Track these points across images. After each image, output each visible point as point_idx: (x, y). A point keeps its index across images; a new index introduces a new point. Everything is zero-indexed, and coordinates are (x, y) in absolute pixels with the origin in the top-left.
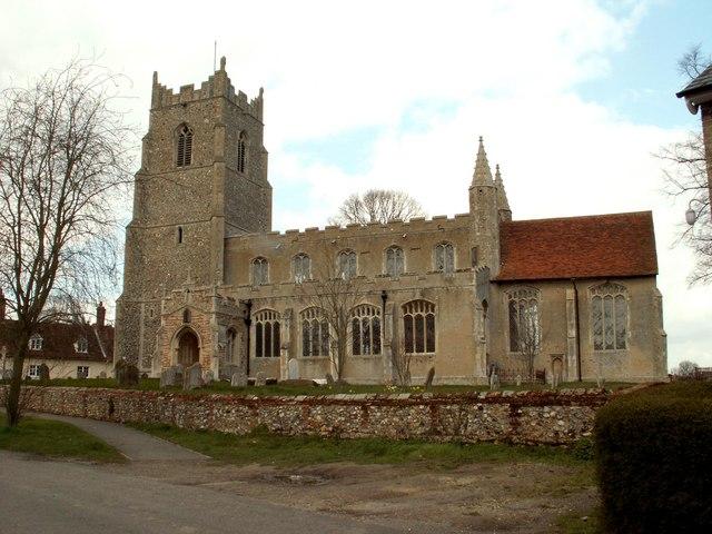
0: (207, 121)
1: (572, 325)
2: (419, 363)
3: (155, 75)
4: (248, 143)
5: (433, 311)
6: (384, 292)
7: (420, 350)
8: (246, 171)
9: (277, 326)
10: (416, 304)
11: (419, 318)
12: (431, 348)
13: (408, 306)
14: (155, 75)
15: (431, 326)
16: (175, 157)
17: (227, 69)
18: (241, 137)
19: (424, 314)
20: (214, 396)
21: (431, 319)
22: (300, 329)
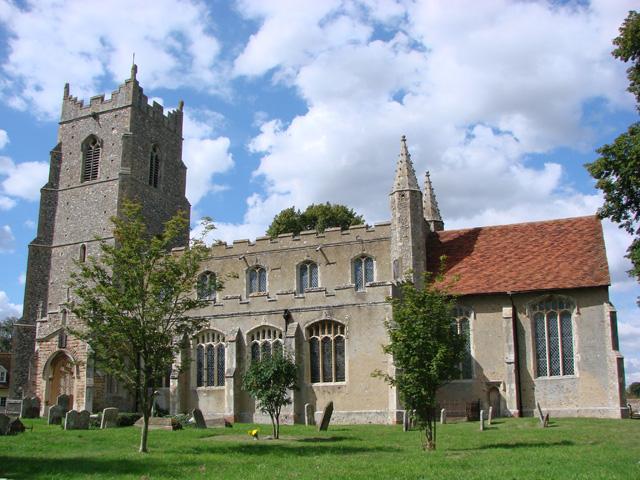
0: (115, 132)
1: (510, 348)
2: (326, 394)
3: (67, 87)
4: (163, 155)
5: (342, 333)
6: (286, 311)
7: (210, 383)
8: (161, 186)
9: (221, 350)
10: (264, 332)
11: (265, 345)
12: (340, 377)
13: (315, 328)
14: (67, 87)
15: (340, 351)
16: (79, 171)
17: (139, 77)
18: (154, 150)
19: (332, 337)
20: (220, 427)
21: (339, 340)
22: (194, 356)
